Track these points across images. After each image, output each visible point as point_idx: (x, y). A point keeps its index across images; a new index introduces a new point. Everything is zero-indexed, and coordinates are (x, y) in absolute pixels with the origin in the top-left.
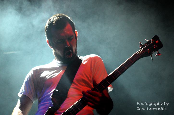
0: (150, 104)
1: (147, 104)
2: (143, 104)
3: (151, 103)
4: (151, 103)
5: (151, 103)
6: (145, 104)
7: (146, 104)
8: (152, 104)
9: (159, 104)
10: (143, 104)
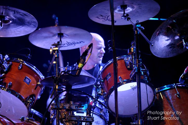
0: (161, 113)
1: (158, 113)
3: (162, 112)
6: (155, 113)
7: (157, 113)
8: (164, 112)
9: (171, 113)
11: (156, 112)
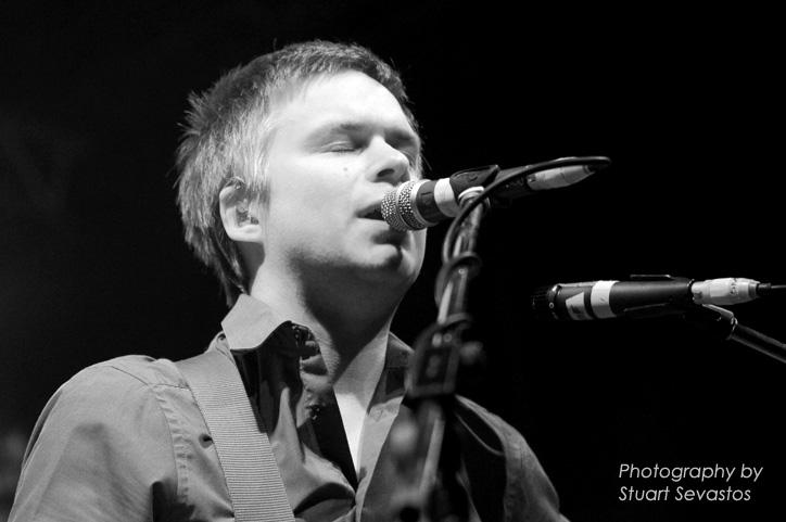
0: (677, 473)
2: (647, 473)
3: (681, 470)
4: (683, 471)
5: (681, 470)
6: (653, 471)
7: (658, 471)
9: (720, 471)
10: (708, 473)
11: (656, 468)
